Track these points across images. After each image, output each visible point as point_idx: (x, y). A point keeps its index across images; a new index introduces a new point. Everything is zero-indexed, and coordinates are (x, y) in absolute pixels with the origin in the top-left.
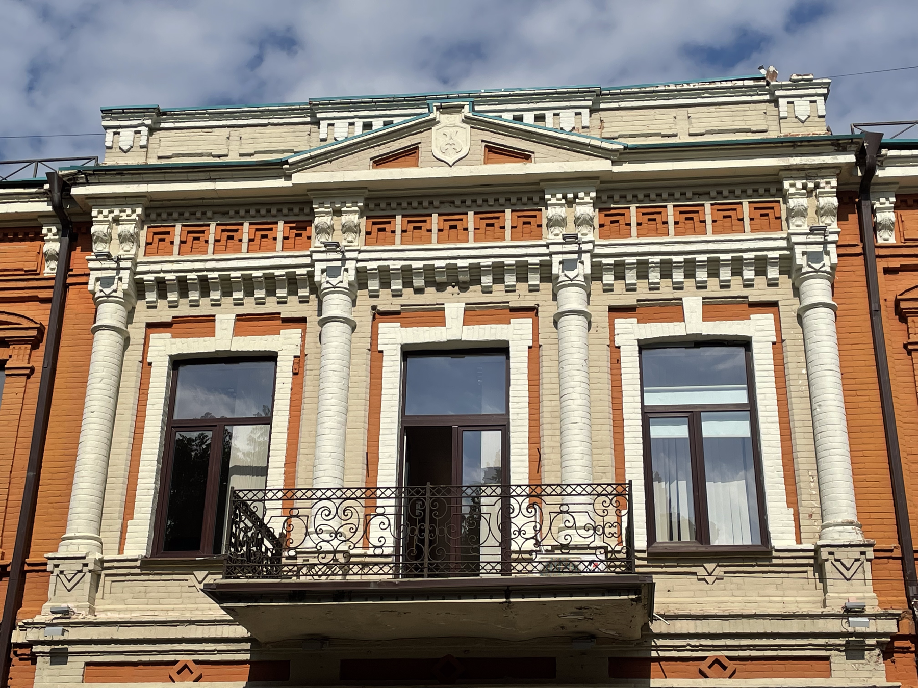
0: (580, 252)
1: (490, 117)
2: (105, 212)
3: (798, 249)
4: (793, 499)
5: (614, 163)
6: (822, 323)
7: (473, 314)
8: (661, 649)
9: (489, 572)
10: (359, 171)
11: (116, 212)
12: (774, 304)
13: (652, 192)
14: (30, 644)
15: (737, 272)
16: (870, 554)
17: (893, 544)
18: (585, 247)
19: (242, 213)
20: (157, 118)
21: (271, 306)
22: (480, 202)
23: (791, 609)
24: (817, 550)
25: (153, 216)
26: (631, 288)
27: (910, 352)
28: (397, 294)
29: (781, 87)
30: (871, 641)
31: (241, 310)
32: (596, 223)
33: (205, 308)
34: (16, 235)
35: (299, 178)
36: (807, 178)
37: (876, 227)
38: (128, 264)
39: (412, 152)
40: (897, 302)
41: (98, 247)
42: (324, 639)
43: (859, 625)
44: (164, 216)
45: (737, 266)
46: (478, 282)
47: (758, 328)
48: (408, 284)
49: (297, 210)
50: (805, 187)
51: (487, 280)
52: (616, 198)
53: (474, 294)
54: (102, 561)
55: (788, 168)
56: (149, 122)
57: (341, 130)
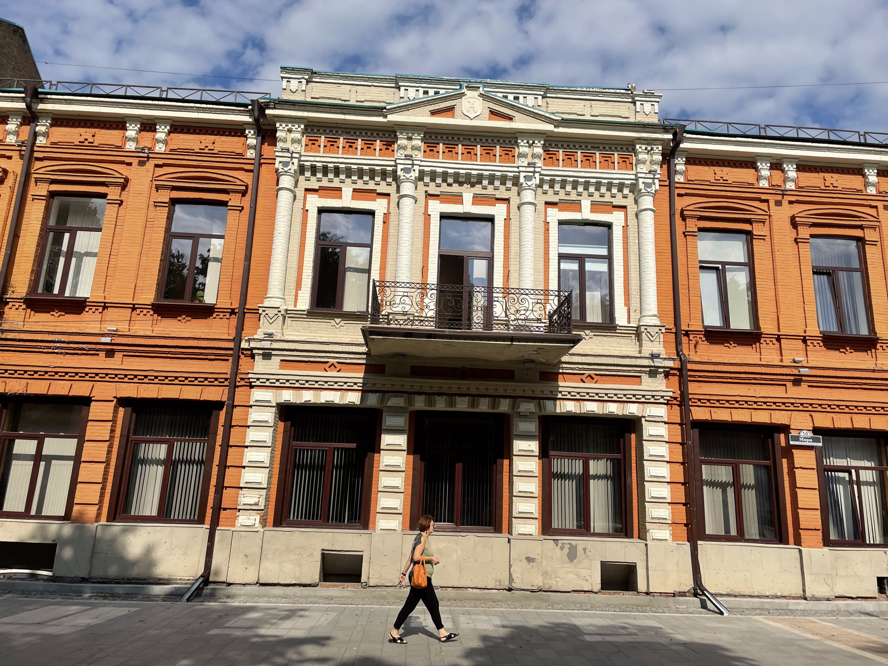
0: (534, 172)
1: (492, 95)
2: (284, 125)
3: (641, 181)
4: (627, 303)
5: (555, 127)
6: (648, 218)
7: (478, 199)
8: (564, 368)
9: (477, 327)
10: (422, 117)
11: (290, 126)
12: (625, 207)
13: (571, 144)
14: (251, 349)
15: (609, 190)
16: (663, 330)
17: (672, 326)
18: (537, 170)
19: (358, 133)
20: (311, 75)
21: (371, 186)
22: (484, 140)
23: (625, 354)
24: (638, 327)
25: (309, 130)
26: (556, 193)
27: (685, 236)
28: (439, 186)
29: (638, 95)
30: (661, 370)
31: (355, 186)
32: (303, 144)
33: (336, 183)
34: (236, 133)
35: (392, 118)
36: (648, 144)
37: (676, 172)
38: (297, 155)
39: (451, 109)
40: (682, 211)
41: (280, 145)
42: (404, 355)
43: (658, 363)
44: (315, 131)
45: (609, 186)
46: (481, 183)
47: (616, 218)
48: (445, 181)
49: (388, 135)
50: (646, 149)
51: (485, 182)
52: (553, 145)
53: (478, 189)
54: (287, 310)
55: (639, 139)
56: (307, 77)
57: (412, 93)
